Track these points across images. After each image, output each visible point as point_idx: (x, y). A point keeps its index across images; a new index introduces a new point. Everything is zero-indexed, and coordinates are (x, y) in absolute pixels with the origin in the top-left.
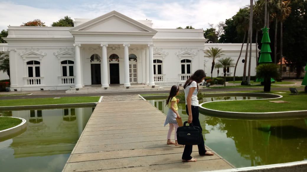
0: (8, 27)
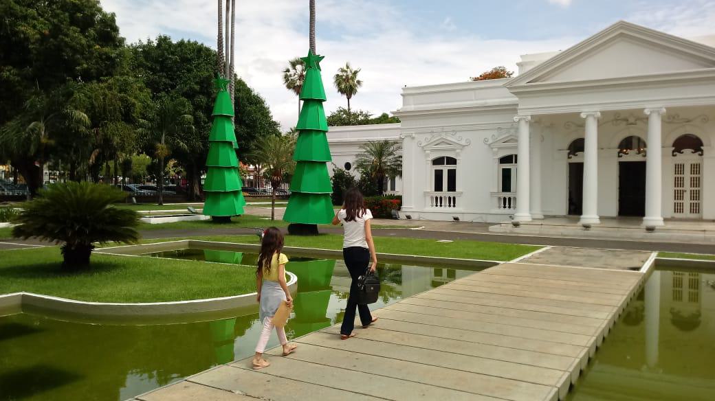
0: (403, 89)
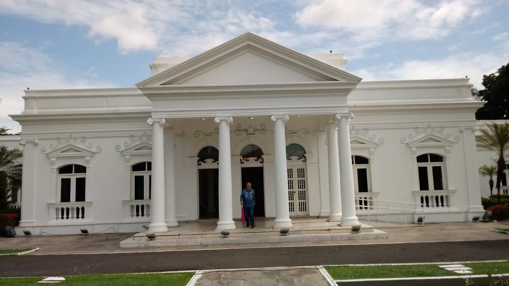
0: (25, 91)
